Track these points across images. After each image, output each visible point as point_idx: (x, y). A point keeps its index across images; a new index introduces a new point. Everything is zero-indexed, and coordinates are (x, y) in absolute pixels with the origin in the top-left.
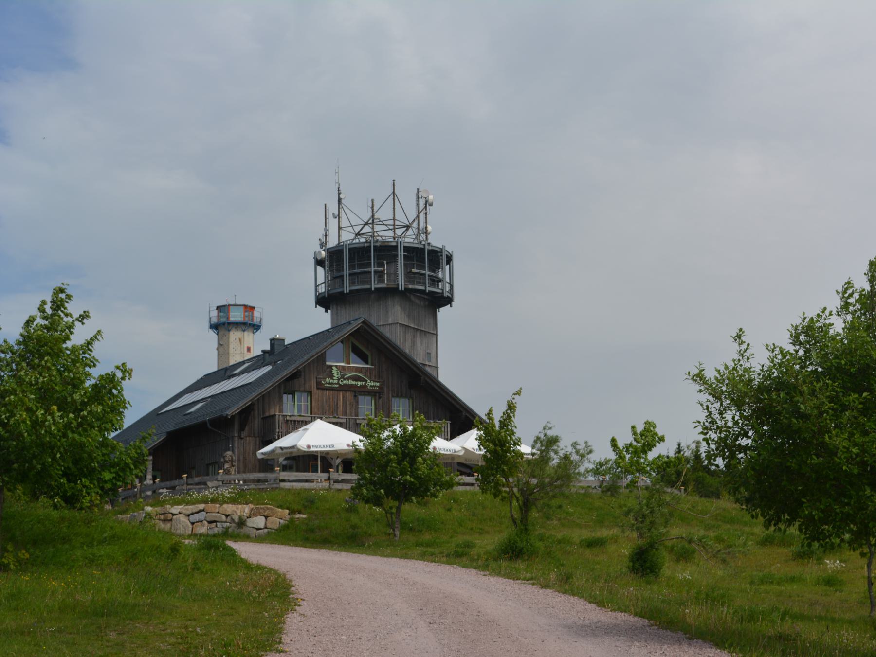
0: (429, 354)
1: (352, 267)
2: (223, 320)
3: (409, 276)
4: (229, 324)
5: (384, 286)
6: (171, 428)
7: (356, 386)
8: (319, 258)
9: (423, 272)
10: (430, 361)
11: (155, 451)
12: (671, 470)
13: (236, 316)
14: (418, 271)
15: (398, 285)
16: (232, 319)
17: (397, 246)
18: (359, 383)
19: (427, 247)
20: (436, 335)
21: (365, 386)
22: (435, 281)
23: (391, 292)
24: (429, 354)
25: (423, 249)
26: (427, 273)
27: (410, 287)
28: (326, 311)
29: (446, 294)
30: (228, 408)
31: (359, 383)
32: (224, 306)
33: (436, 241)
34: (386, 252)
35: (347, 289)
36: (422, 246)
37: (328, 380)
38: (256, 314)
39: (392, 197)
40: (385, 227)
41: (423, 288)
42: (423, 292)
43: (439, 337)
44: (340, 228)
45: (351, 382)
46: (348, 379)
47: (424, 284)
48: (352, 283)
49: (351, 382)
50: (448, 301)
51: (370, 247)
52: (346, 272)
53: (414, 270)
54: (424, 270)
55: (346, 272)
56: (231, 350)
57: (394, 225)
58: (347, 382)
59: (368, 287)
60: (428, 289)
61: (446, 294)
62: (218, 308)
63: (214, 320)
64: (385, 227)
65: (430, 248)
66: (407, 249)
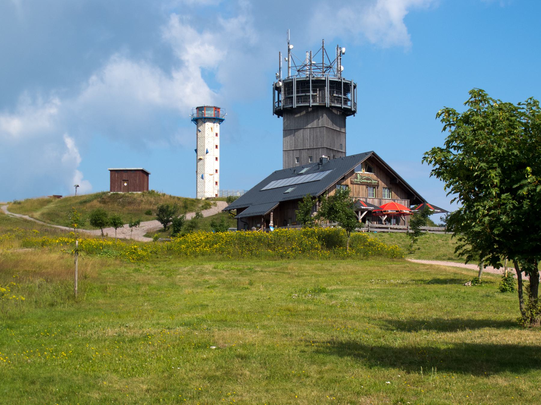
0: (341, 144)
1: (298, 92)
2: (200, 116)
3: (333, 99)
4: (205, 118)
5: (318, 104)
6: (281, 200)
7: (367, 183)
8: (278, 86)
9: (340, 96)
10: (341, 149)
11: (275, 211)
12: (246, 226)
13: (209, 114)
14: (337, 95)
15: (326, 104)
16: (206, 116)
17: (325, 80)
18: (369, 181)
19: (343, 81)
20: (345, 133)
21: (371, 183)
22: (346, 100)
23: (321, 108)
24: (341, 144)
25: (341, 82)
26: (343, 96)
27: (333, 105)
28: (279, 117)
29: (353, 109)
30: (316, 193)
31: (369, 181)
32: (202, 107)
33: (347, 78)
34: (319, 84)
35: (295, 105)
36: (340, 80)
37: (356, 180)
38: (221, 112)
39: (322, 50)
40: (316, 67)
41: (340, 106)
42: (340, 108)
43: (347, 135)
44: (289, 67)
45: (365, 181)
46: (364, 179)
47: (341, 103)
48: (298, 102)
49: (365, 181)
50: (353, 113)
51: (309, 80)
52: (295, 95)
53: (335, 95)
54: (341, 94)
55: (295, 95)
56: (206, 135)
57: (323, 66)
58: (363, 181)
59: (308, 104)
60: (343, 106)
61: (353, 109)
62: (197, 108)
63: (195, 116)
64: (316, 67)
65: (345, 81)
66: (332, 82)
